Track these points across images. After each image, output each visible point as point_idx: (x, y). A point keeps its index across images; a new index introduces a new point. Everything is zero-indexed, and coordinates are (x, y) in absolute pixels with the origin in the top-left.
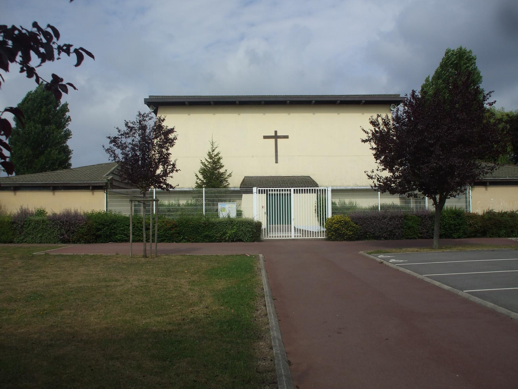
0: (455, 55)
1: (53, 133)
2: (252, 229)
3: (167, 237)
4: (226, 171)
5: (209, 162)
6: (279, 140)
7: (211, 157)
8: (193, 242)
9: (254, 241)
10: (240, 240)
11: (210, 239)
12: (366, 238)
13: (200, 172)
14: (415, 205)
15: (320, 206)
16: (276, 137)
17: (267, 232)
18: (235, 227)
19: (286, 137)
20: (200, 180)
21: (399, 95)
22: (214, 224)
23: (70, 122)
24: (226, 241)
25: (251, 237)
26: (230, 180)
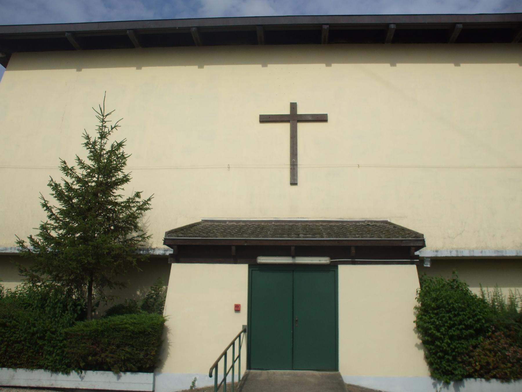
6: (302, 127)
19: (322, 119)
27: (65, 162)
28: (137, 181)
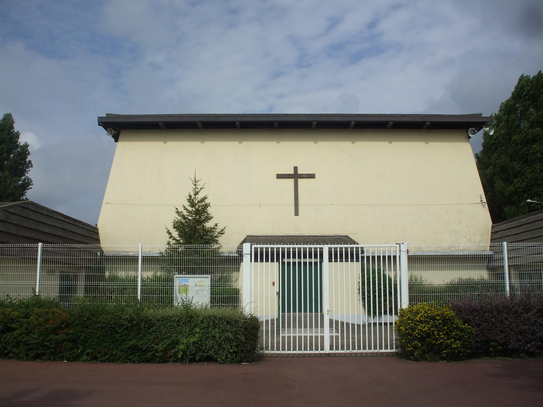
0: (531, 83)
1: (6, 181)
2: (236, 333)
3: (49, 348)
4: (216, 225)
5: (190, 212)
6: (300, 181)
7: (193, 205)
8: (104, 361)
9: (241, 361)
10: (210, 359)
11: (142, 355)
12: (487, 353)
13: (175, 227)
14: (518, 281)
15: (369, 283)
16: (296, 176)
17: (278, 327)
18: (197, 330)
19: (312, 176)
20: (174, 239)
21: (481, 114)
22: (150, 323)
23: (30, 169)
24: (177, 361)
25: (234, 352)
26: (221, 239)
27: (177, 209)
28: (217, 217)
